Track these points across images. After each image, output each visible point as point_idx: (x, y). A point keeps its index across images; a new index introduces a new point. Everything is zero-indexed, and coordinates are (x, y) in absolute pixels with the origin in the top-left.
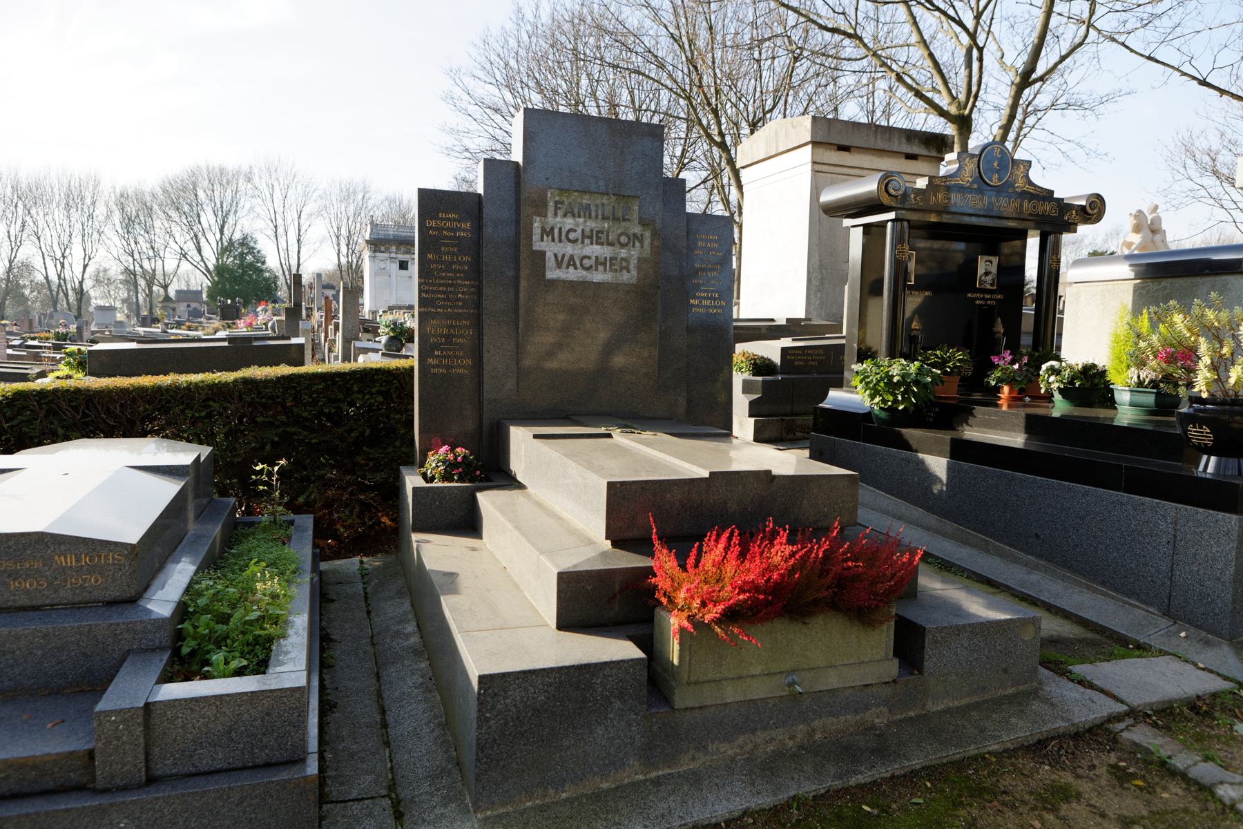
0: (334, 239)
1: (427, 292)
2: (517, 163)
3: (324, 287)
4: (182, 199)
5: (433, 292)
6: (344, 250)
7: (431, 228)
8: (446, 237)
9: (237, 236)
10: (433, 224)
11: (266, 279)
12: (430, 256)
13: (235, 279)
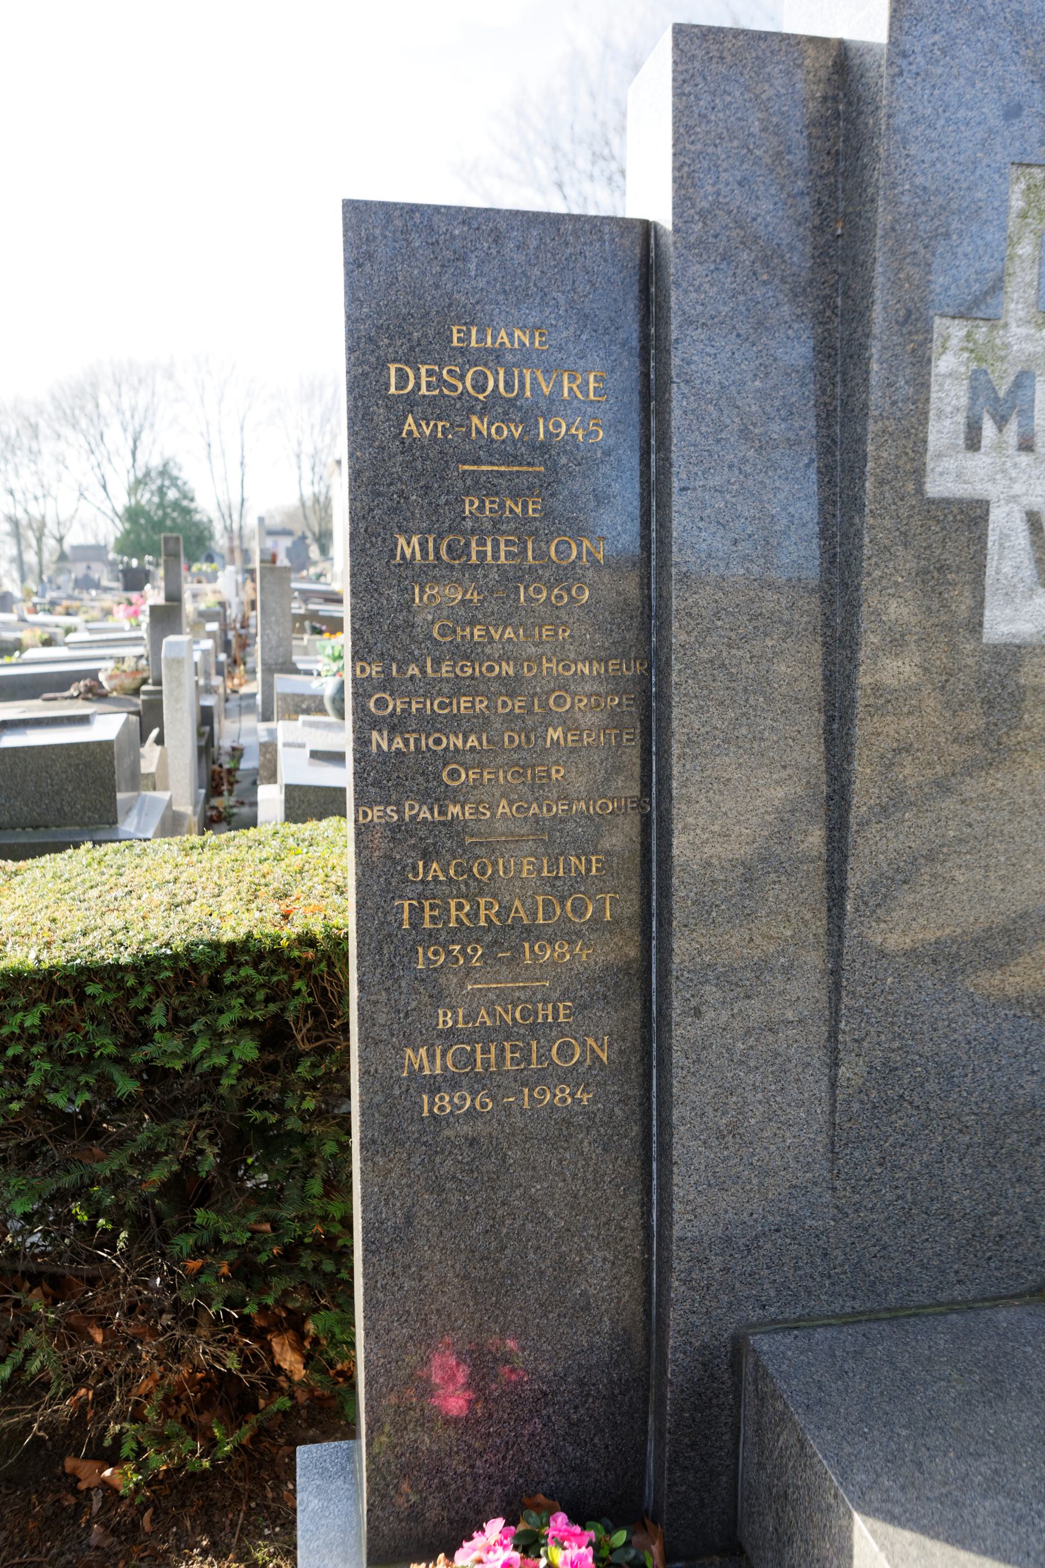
0: (294, 459)
1: (395, 725)
2: (647, 229)
3: (271, 533)
4: (78, 407)
5: (429, 723)
6: (307, 475)
7: (411, 402)
8: (491, 450)
9: (156, 462)
10: (421, 380)
11: (197, 525)
12: (408, 547)
13: (158, 526)
